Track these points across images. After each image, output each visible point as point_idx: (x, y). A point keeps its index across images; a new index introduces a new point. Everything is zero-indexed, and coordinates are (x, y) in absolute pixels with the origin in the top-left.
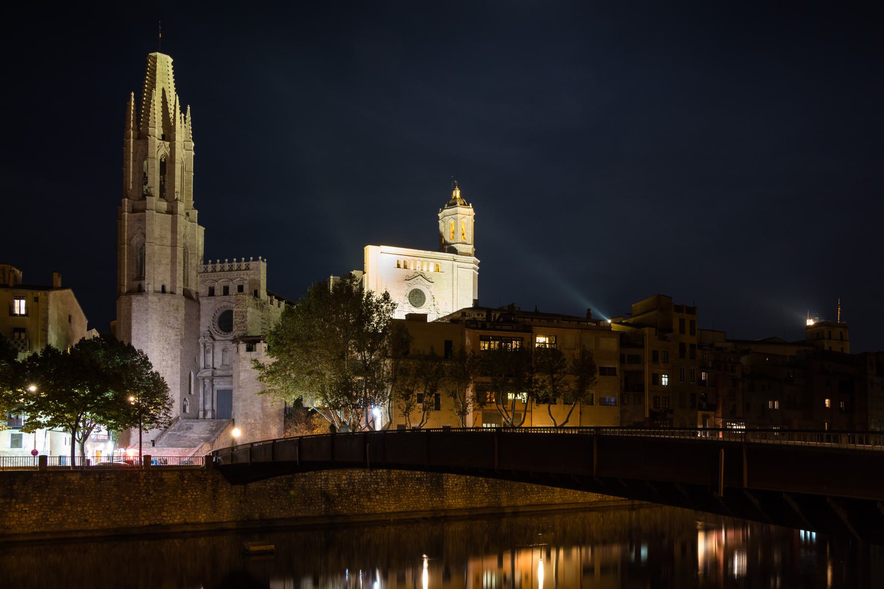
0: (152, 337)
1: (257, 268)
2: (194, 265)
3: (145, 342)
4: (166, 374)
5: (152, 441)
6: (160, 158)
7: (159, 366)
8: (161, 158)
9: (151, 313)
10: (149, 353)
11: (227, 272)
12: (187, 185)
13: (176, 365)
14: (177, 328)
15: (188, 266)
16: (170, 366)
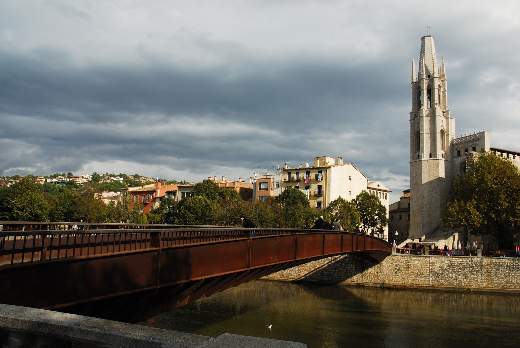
4: (432, 202)
13: (437, 197)
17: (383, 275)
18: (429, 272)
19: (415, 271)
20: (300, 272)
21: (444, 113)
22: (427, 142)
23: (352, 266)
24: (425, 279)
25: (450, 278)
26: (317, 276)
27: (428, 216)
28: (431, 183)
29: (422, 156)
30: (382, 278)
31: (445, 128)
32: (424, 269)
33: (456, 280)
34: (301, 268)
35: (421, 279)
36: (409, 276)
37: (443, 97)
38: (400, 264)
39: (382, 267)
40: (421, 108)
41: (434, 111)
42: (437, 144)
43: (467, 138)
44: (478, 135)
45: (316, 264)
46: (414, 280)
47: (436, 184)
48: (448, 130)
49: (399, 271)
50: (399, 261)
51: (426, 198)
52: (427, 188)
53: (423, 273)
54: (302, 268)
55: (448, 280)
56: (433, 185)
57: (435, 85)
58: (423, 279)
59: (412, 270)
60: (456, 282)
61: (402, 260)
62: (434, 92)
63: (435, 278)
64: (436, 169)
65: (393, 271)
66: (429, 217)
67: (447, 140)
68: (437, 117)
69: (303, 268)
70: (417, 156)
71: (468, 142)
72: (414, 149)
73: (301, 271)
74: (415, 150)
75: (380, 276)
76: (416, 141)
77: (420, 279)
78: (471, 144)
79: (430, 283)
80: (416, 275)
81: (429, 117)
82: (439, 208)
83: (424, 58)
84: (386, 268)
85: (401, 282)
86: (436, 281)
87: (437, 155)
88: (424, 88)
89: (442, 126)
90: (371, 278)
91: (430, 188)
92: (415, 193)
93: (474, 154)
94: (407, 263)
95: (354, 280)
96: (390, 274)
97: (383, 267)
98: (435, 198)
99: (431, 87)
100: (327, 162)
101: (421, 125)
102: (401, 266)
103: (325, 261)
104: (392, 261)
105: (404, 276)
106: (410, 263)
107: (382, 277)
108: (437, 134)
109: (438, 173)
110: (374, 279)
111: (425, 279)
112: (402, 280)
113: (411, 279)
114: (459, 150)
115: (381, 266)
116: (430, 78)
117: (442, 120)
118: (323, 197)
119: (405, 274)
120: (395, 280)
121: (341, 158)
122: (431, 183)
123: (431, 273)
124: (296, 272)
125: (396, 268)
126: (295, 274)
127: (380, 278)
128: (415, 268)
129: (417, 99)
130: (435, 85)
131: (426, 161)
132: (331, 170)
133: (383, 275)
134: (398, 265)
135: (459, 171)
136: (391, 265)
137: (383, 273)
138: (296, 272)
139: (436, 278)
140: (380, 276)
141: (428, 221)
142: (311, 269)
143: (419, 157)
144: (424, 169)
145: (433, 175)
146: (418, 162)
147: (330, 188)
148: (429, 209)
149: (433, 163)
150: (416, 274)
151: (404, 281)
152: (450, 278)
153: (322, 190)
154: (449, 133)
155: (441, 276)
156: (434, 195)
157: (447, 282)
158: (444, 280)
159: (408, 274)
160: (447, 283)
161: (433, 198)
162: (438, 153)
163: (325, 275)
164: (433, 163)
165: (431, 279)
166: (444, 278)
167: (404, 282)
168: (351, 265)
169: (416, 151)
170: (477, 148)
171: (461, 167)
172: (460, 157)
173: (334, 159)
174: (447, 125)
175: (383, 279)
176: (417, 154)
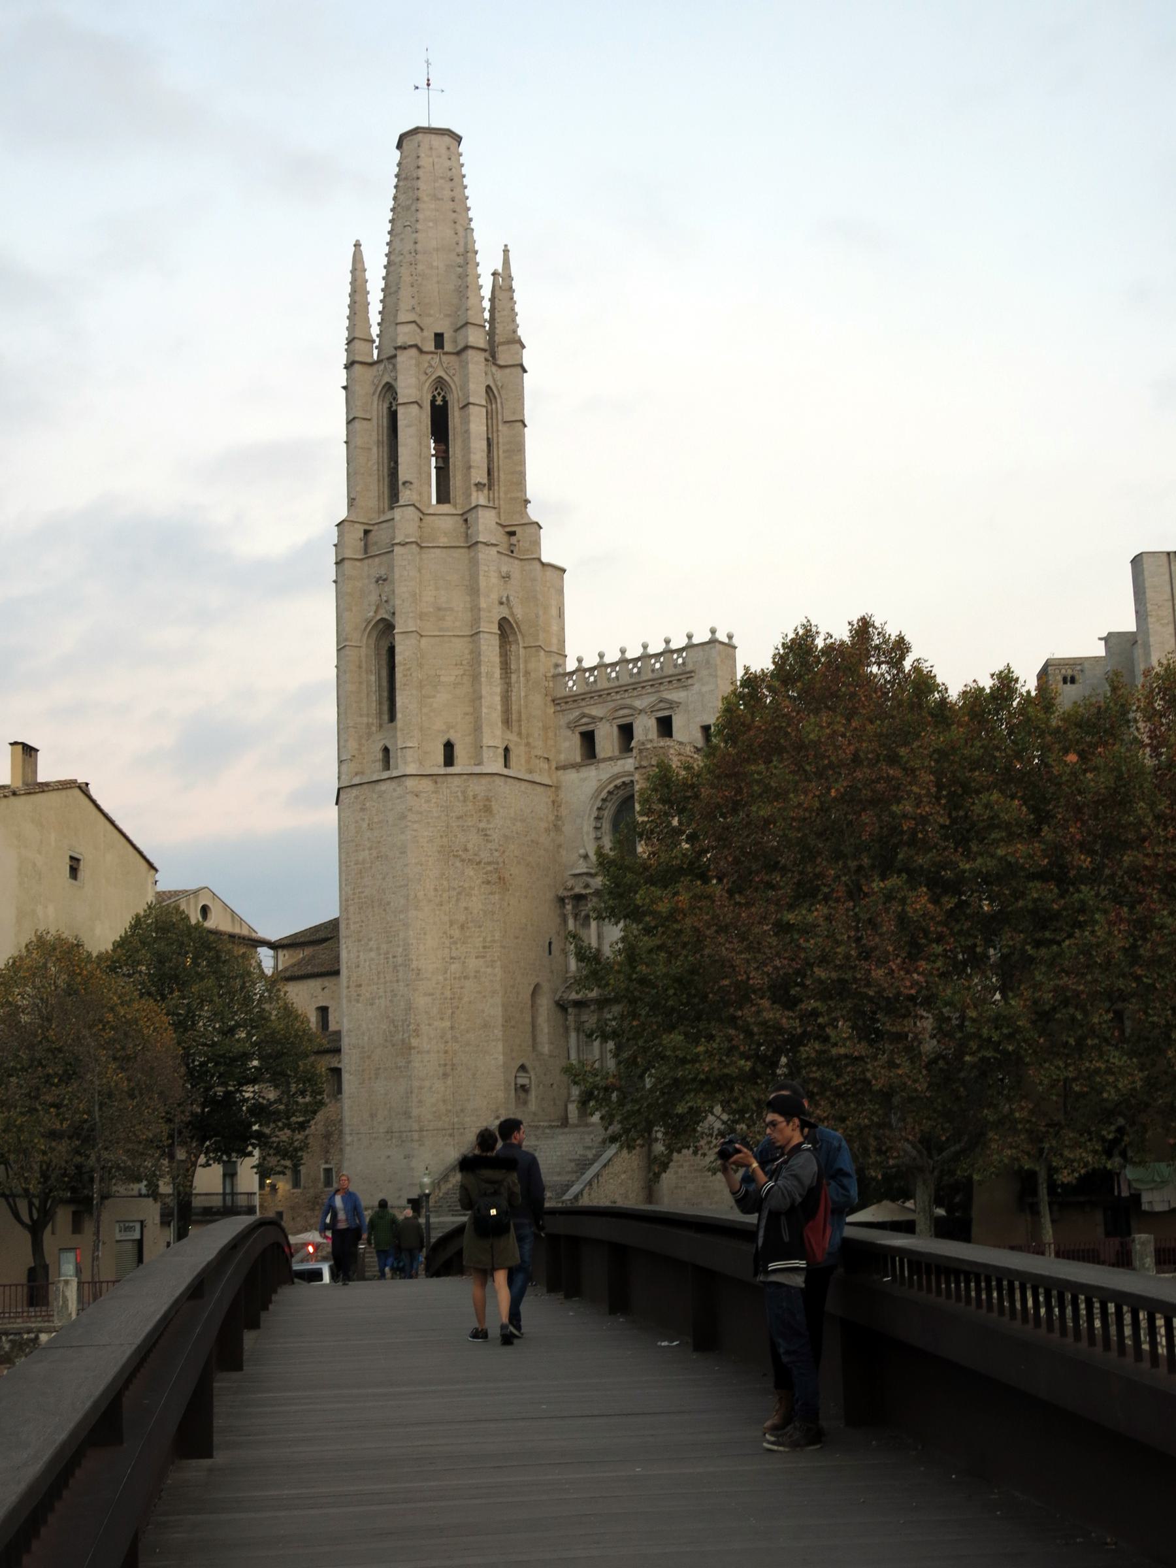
0: (421, 894)
1: (708, 662)
2: (536, 735)
3: (401, 911)
4: (460, 999)
5: (410, 1201)
6: (430, 397)
7: (441, 978)
8: (434, 396)
9: (416, 826)
10: (414, 941)
11: (582, 1186)
12: (506, 458)
13: (489, 970)
14: (489, 863)
15: (518, 682)
16: (472, 974)
27: (445, 1075)
28: (458, 900)
44: (639, 668)
47: (480, 906)
51: (429, 979)
52: (435, 923)
56: (466, 909)
66: (449, 1082)
70: (380, 755)
71: (636, 686)
72: (361, 716)
74: (365, 720)
76: (369, 671)
82: (498, 1032)
89: (504, 599)
91: (451, 923)
92: (371, 950)
98: (476, 977)
114: (590, 728)
116: (442, 348)
122: (458, 900)
129: (375, 450)
135: (592, 835)
141: (444, 1101)
146: (383, 787)
148: (449, 1036)
149: (463, 792)
156: (473, 963)
161: (466, 978)
169: (368, 725)
171: (598, 818)
172: (593, 767)
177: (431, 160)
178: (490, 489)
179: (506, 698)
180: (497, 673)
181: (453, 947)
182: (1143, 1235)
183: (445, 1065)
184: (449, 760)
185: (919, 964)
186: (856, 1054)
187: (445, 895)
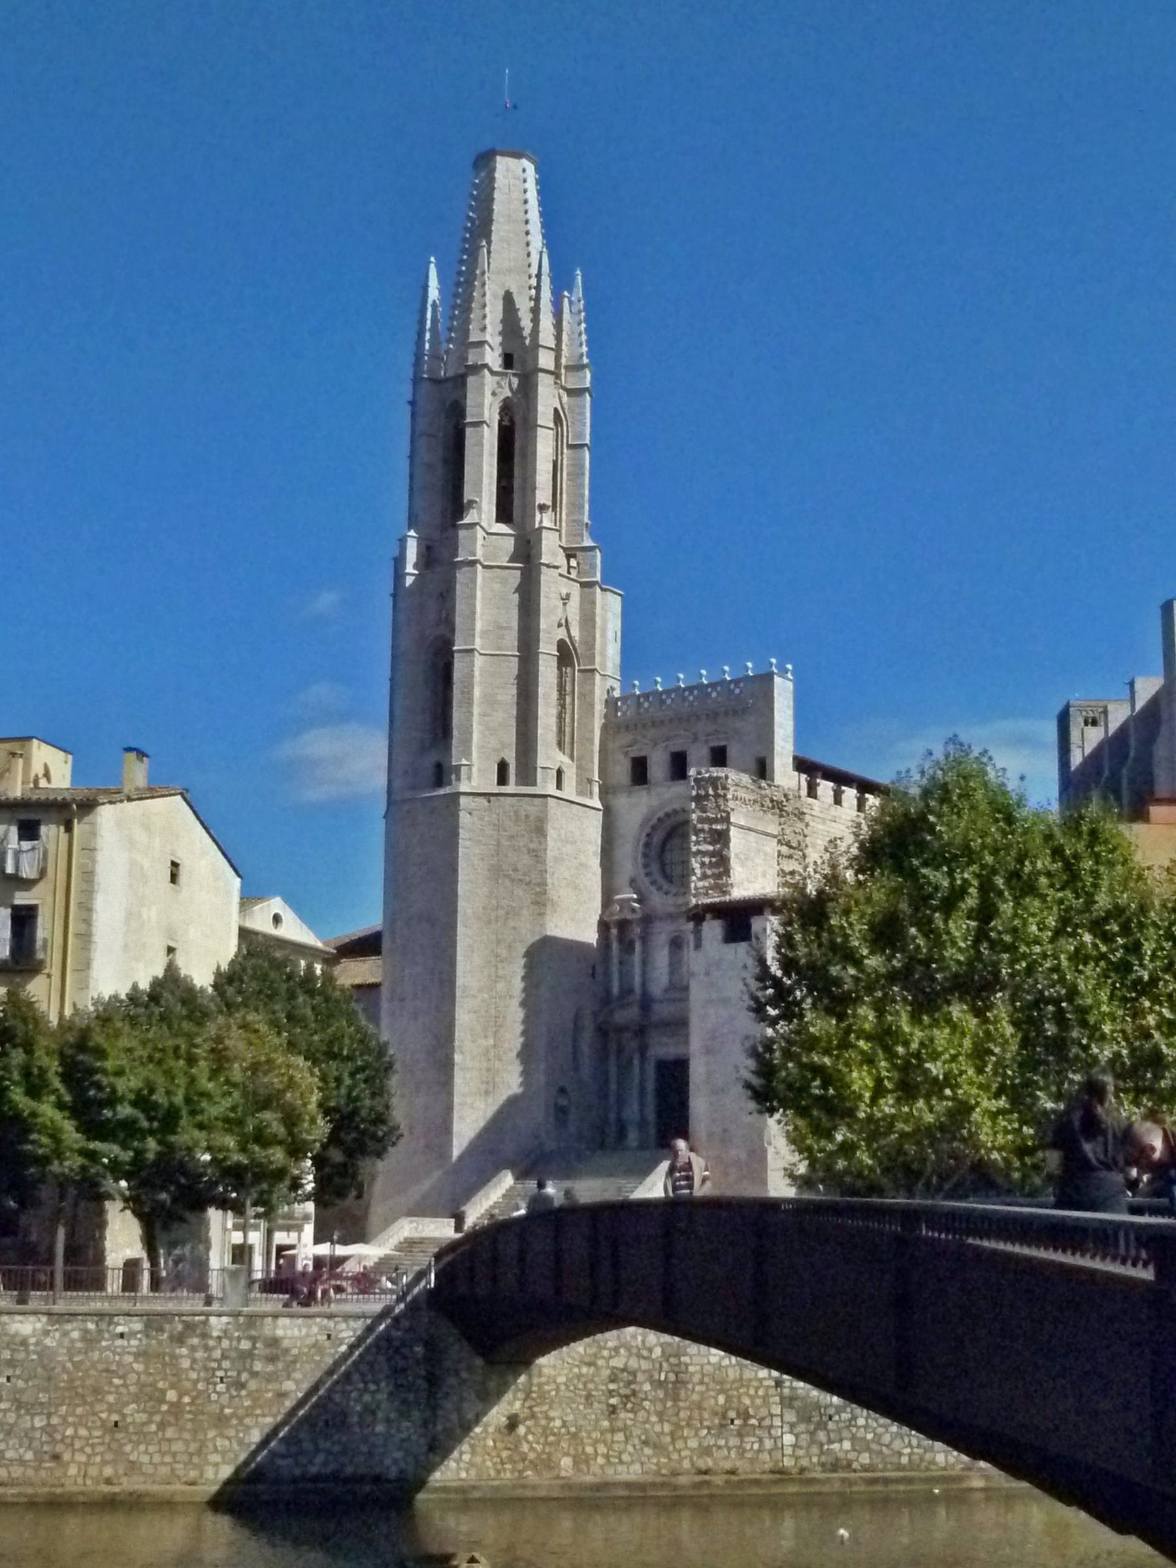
17: (545, 1429)
18: (777, 1399)
19: (712, 1402)
20: (62, 1441)
21: (574, 556)
22: (490, 701)
23: (372, 1387)
24: (761, 1441)
25: (880, 1430)
26: (168, 1459)
29: (464, 770)
30: (539, 1448)
31: (575, 632)
32: (757, 1389)
33: (906, 1441)
34: (64, 1418)
35: (742, 1441)
36: (682, 1428)
37: (568, 475)
38: (633, 1363)
39: (540, 1385)
40: (462, 519)
41: (529, 542)
42: (540, 713)
43: (684, 699)
45: (161, 1385)
46: (706, 1451)
48: (590, 643)
49: (629, 1406)
50: (628, 1348)
53: (751, 1412)
54: (73, 1414)
55: (873, 1440)
57: (540, 408)
58: (752, 1444)
59: (695, 1397)
60: (908, 1450)
61: (643, 1342)
62: (531, 442)
63: (808, 1432)
64: (532, 846)
65: (596, 1405)
67: (582, 696)
68: (543, 577)
69: (79, 1410)
73: (69, 1432)
75: (530, 1437)
77: (734, 1441)
78: (703, 727)
79: (788, 1462)
80: (717, 1421)
81: (518, 573)
83: (489, 264)
84: (557, 1390)
85: (642, 1464)
86: (815, 1450)
87: (539, 770)
88: (482, 414)
89: (563, 621)
90: (479, 1450)
91: (499, 942)
93: (730, 781)
94: (670, 1356)
95: (388, 1468)
96: (581, 1422)
97: (547, 1388)
99: (518, 420)
100: (37, 776)
101: (460, 607)
102: (640, 1377)
103: (214, 1365)
104: (594, 1350)
105: (658, 1428)
106: (682, 1359)
107: (542, 1440)
108: (541, 662)
109: (540, 867)
110: (499, 1456)
111: (761, 1441)
112: (648, 1451)
113: (693, 1443)
115: (535, 1381)
117: (564, 592)
118: (49, 976)
119: (661, 1421)
120: (607, 1457)
121: (141, 754)
123: (792, 1407)
124: (31, 1439)
125: (612, 1386)
126: (29, 1456)
127: (532, 1449)
128: (712, 1385)
130: (540, 408)
131: (483, 801)
132: (99, 820)
133: (545, 1429)
134: (623, 1370)
136: (585, 1370)
137: (543, 1422)
138: (36, 1444)
139: (812, 1434)
140: (530, 1437)
142: (129, 1420)
143: (442, 774)
144: (468, 843)
145: (514, 875)
147: (88, 922)
149: (516, 813)
150: (716, 1414)
151: (655, 1461)
152: (880, 1430)
153: (41, 934)
154: (594, 663)
155: (836, 1418)
157: (869, 1449)
158: (853, 1438)
159: (674, 1419)
160: (867, 1455)
162: (541, 762)
163: (216, 1450)
164: (516, 813)
165: (789, 1439)
166: (854, 1430)
167: (657, 1464)
168: (366, 1383)
170: (733, 753)
173: (70, 757)
174: (588, 619)
175: (543, 1452)
176: (433, 757)
177: (506, 181)
178: (554, 509)
179: (560, 718)
180: (555, 695)
181: (500, 965)
182: (801, 1384)
183: (487, 1083)
184: (502, 780)
185: (790, 1192)
186: (349, 1470)
187: (493, 914)
